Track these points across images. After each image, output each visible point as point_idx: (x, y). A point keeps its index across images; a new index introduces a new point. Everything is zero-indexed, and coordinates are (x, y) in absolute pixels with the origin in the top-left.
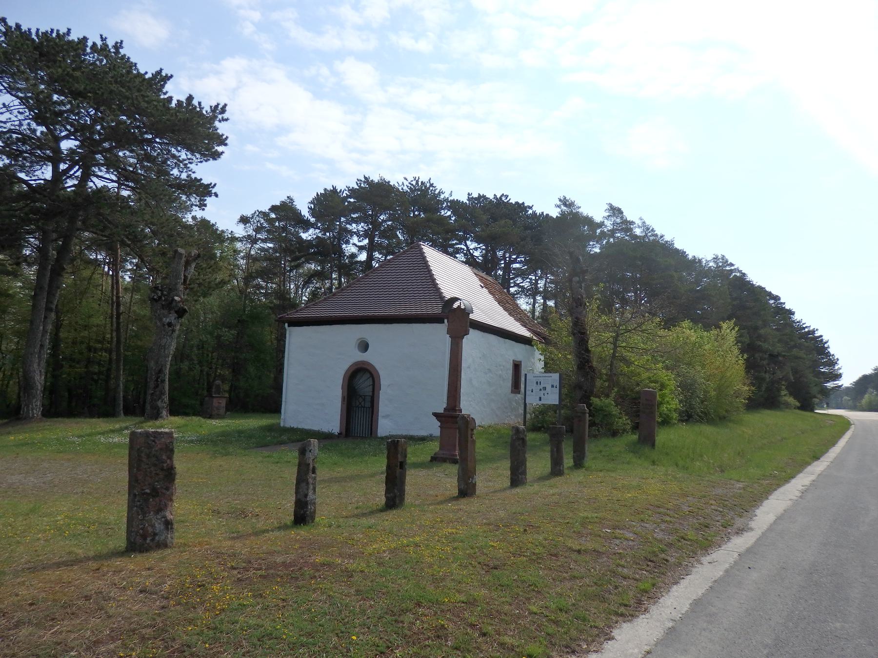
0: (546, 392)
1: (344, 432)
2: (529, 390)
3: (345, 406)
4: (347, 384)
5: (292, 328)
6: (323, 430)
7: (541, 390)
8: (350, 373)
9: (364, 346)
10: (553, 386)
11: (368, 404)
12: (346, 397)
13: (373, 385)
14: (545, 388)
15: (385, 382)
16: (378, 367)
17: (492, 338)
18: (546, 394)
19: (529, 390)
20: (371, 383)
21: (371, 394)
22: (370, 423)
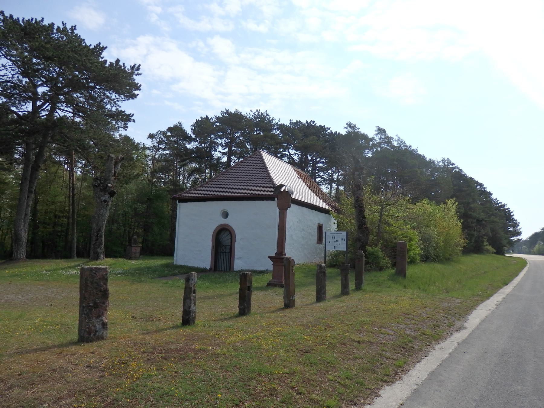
0: (338, 243)
1: (213, 268)
2: (328, 242)
3: (214, 252)
4: (215, 238)
5: (181, 204)
6: (200, 267)
7: (335, 242)
8: (217, 231)
9: (226, 215)
10: (342, 239)
11: (228, 251)
12: (214, 246)
13: (231, 239)
14: (337, 241)
15: (238, 237)
16: (234, 227)
17: (305, 210)
18: (338, 244)
19: (328, 242)
20: (230, 238)
21: (230, 244)
22: (229, 262)
